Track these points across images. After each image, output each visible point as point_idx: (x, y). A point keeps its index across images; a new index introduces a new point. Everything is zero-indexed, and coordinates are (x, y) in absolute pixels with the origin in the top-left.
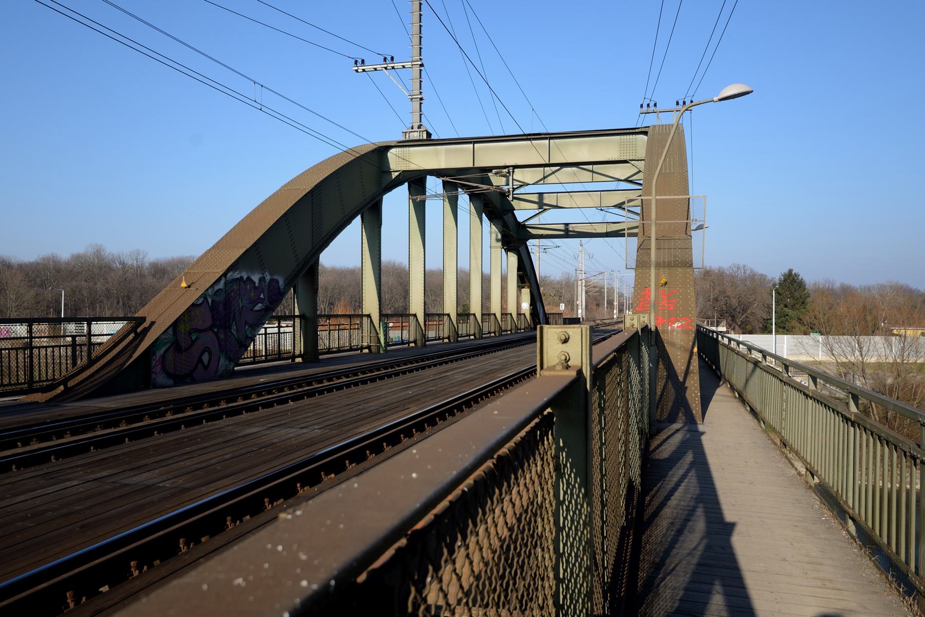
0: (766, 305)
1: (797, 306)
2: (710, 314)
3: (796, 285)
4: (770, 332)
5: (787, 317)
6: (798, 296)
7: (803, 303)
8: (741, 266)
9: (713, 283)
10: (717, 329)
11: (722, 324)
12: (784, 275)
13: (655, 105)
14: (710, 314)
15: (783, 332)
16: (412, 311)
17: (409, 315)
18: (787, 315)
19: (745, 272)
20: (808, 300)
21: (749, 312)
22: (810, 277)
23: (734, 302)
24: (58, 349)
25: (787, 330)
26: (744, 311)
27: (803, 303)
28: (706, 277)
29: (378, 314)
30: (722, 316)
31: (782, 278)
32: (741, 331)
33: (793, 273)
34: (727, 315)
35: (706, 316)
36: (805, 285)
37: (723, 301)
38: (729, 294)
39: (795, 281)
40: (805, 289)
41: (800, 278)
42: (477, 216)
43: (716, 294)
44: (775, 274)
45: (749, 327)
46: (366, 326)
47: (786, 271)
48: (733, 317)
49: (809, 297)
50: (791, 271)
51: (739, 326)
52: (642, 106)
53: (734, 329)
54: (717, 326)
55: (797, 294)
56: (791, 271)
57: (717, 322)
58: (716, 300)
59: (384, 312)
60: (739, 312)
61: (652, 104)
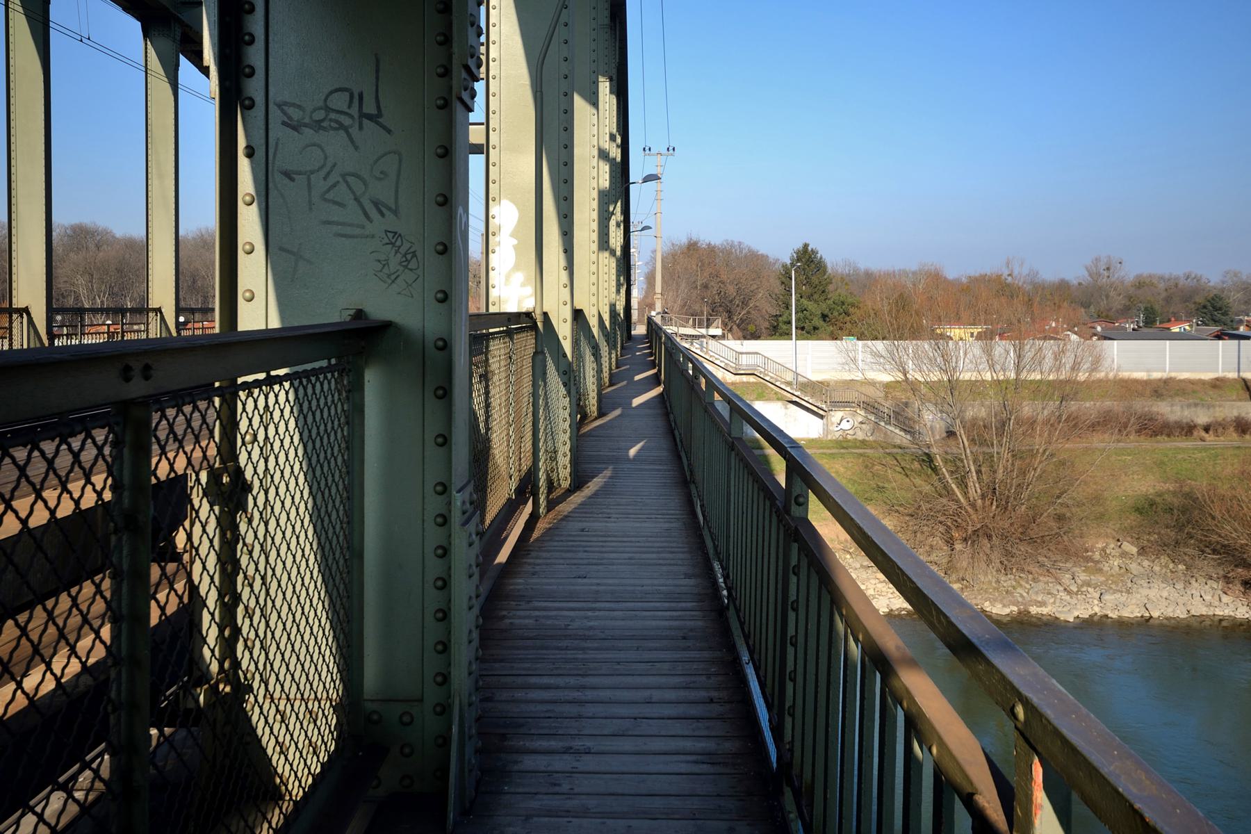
0: (774, 296)
1: (816, 296)
2: (697, 307)
3: (814, 266)
4: (786, 335)
5: (805, 312)
6: (817, 282)
7: (823, 292)
8: (736, 244)
9: (701, 261)
10: (707, 332)
11: (715, 324)
12: (797, 252)
13: (650, 149)
14: (697, 308)
15: (803, 335)
16: (154, 304)
17: (148, 310)
18: (805, 310)
19: (741, 252)
20: (831, 287)
21: (751, 305)
22: (834, 256)
23: (731, 290)
24: (125, 326)
25: (808, 333)
26: (745, 303)
27: (823, 292)
28: (691, 252)
29: (174, 308)
30: (714, 311)
31: (795, 255)
32: (740, 334)
33: (810, 248)
34: (721, 309)
35: (691, 311)
36: (825, 267)
37: (715, 289)
38: (724, 277)
39: (812, 261)
40: (825, 272)
41: (819, 255)
42: (166, 80)
43: (705, 277)
44: (781, 251)
45: (751, 328)
46: (154, 327)
47: (799, 246)
48: (730, 313)
49: (831, 283)
50: (806, 246)
51: (738, 326)
52: (644, 149)
53: (730, 330)
54: (708, 327)
55: (815, 280)
56: (806, 246)
57: (708, 320)
58: (706, 287)
59: (182, 304)
60: (738, 306)
61: (647, 148)
